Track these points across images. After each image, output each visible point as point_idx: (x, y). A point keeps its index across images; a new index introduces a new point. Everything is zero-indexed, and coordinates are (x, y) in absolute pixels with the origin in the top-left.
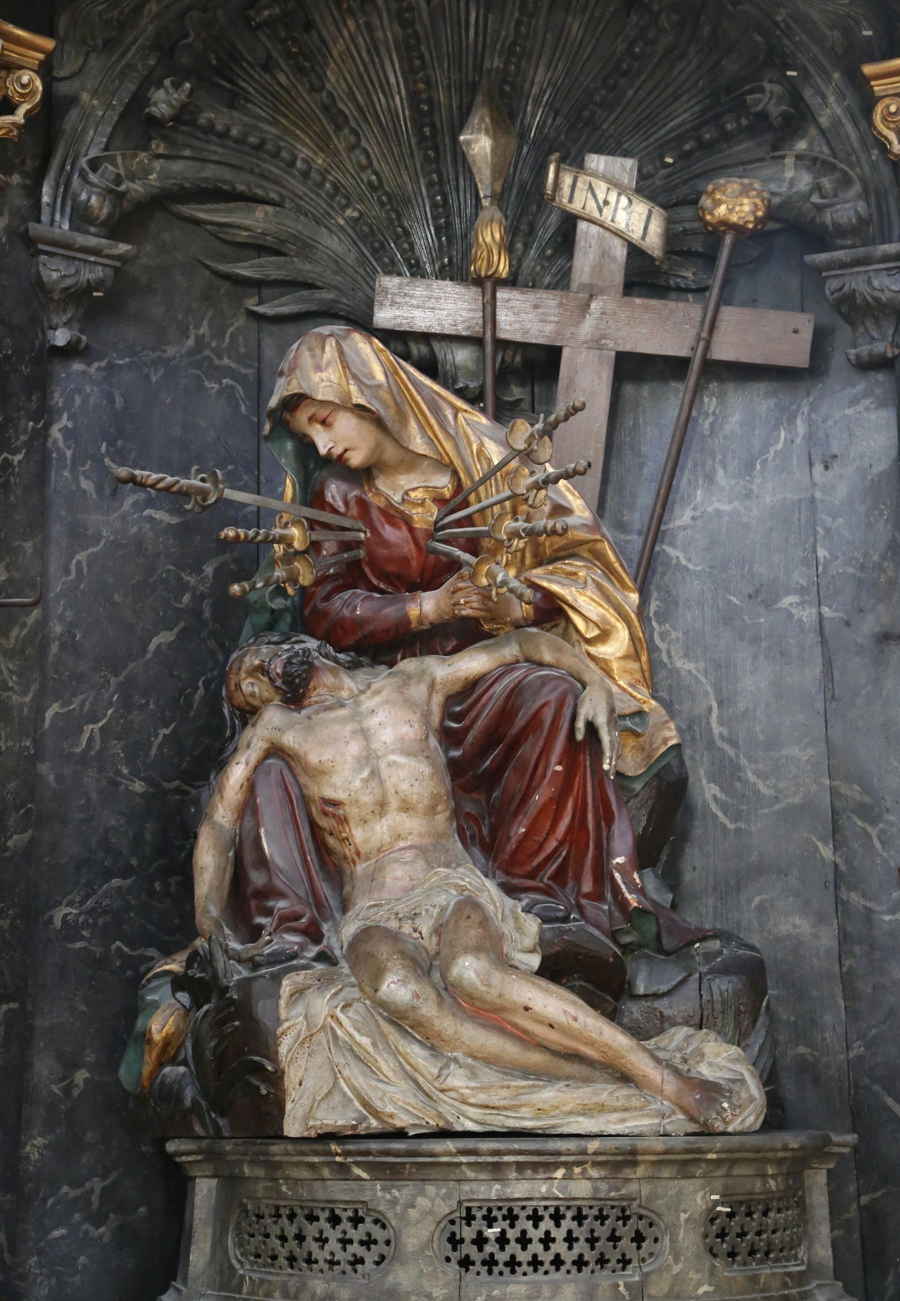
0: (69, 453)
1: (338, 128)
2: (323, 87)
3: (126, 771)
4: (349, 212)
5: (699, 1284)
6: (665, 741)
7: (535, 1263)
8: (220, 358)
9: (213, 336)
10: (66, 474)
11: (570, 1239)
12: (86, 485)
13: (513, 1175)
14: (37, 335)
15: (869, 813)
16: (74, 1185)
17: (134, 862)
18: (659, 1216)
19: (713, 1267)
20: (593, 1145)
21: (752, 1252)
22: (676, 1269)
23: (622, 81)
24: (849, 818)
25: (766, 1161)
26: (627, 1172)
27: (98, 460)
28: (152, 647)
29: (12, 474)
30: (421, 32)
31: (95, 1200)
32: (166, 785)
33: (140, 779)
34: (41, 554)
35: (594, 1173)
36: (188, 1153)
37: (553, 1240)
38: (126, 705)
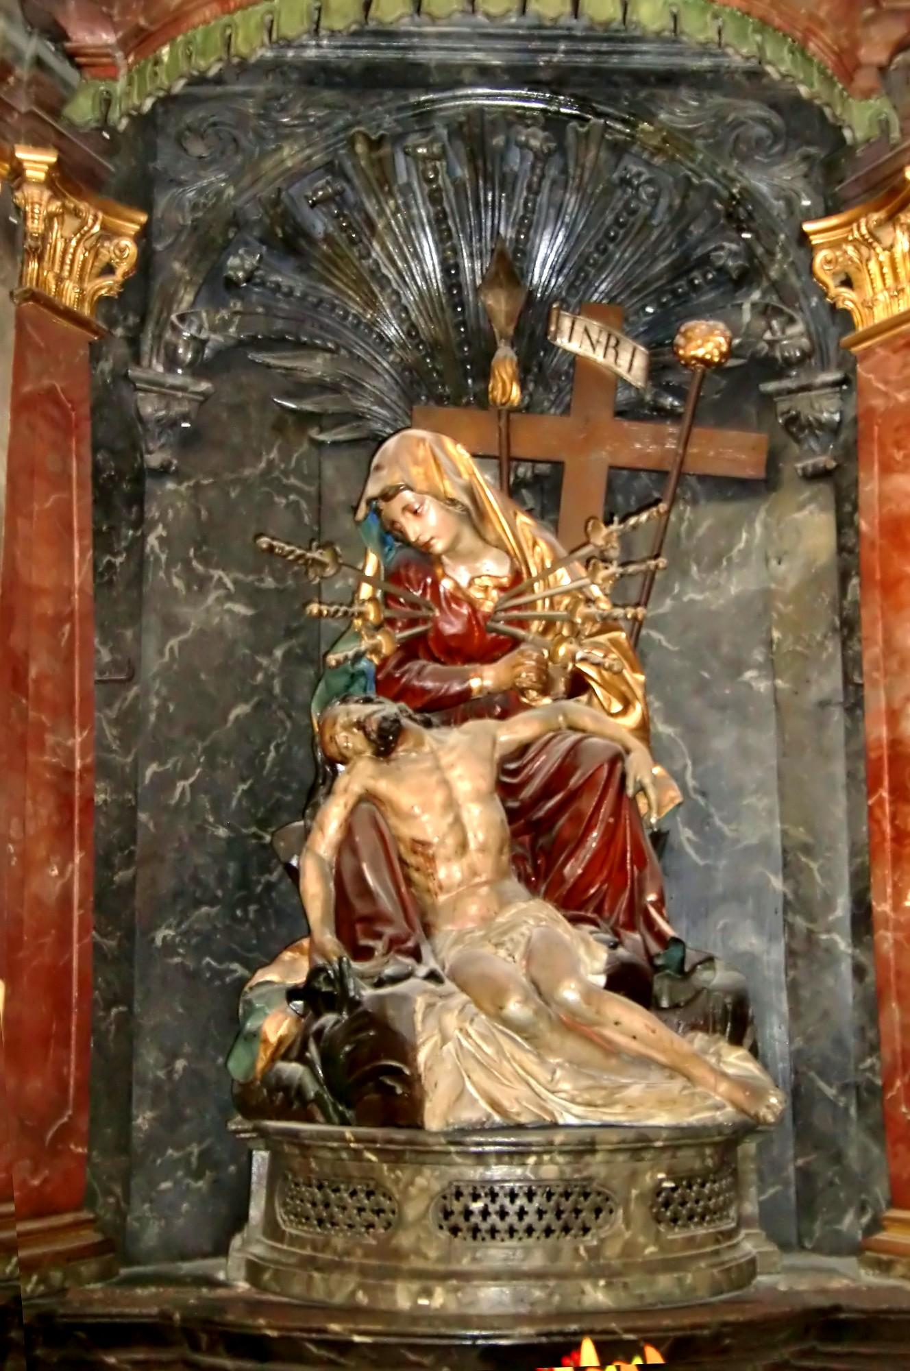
0: (163, 557)
1: (383, 288)
2: (369, 255)
3: (211, 819)
4: (391, 357)
5: (646, 1246)
6: (672, 799)
7: (512, 1231)
8: (288, 478)
9: (282, 460)
10: (162, 574)
11: (541, 1213)
12: (177, 583)
13: (492, 1160)
14: (135, 459)
15: (807, 849)
16: (178, 1147)
17: (220, 893)
18: (615, 1192)
19: (658, 1232)
20: (559, 1137)
21: (690, 1218)
22: (627, 1235)
23: (611, 247)
24: (795, 855)
25: (703, 1145)
26: (588, 1158)
27: (187, 563)
28: (232, 717)
29: (115, 573)
30: (448, 210)
31: (194, 1160)
32: (244, 831)
33: (223, 826)
34: (138, 639)
35: (560, 1159)
36: (245, 1131)
37: (526, 1213)
38: (211, 765)
